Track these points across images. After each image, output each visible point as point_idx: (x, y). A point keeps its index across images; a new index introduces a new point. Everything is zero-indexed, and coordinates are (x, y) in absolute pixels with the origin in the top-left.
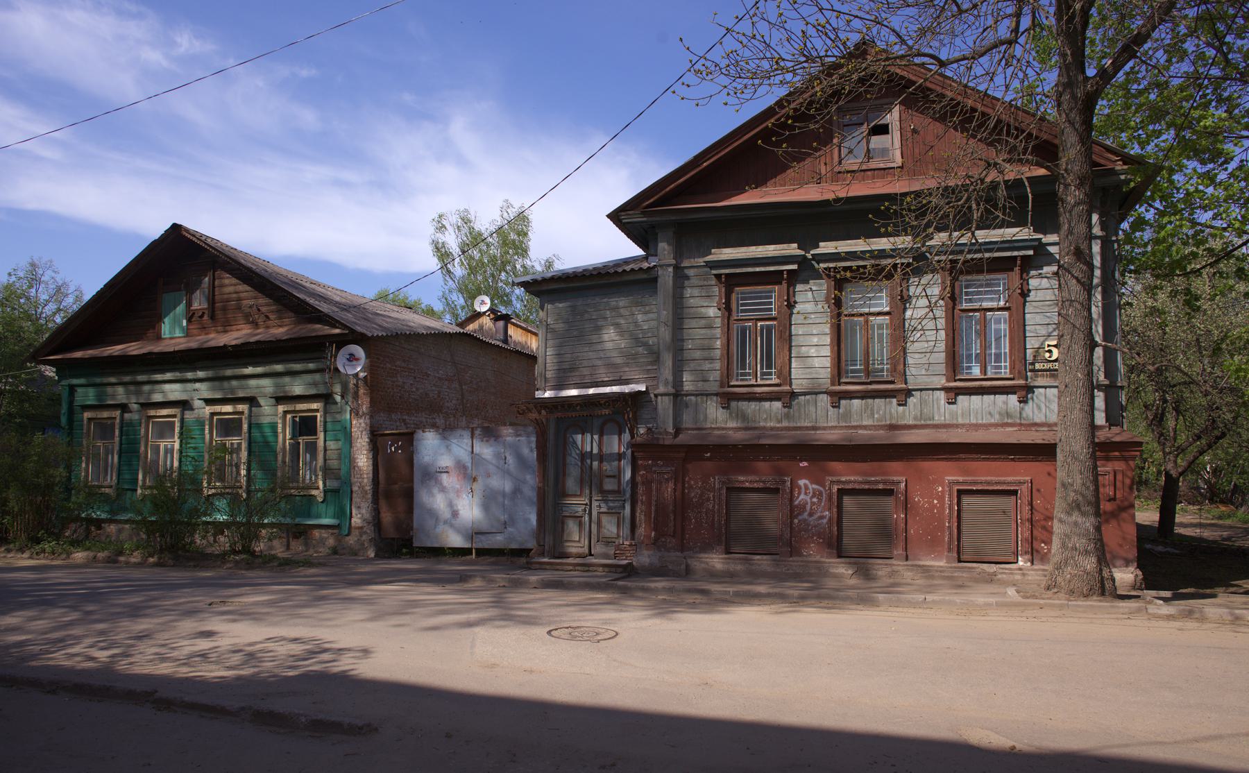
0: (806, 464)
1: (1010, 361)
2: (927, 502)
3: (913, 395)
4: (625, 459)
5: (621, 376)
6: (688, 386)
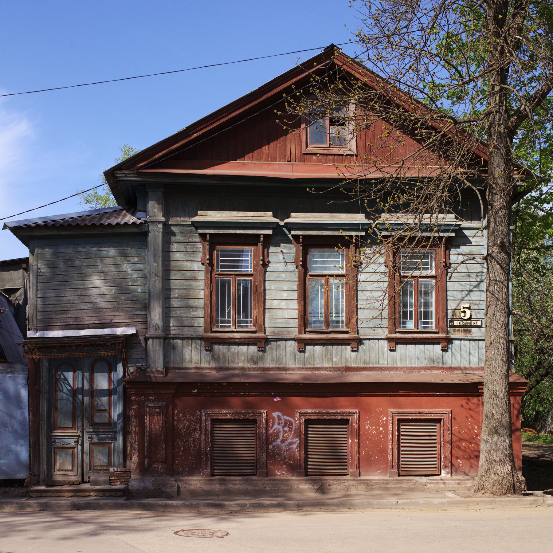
0: (278, 399)
1: (436, 319)
2: (375, 429)
3: (363, 344)
4: (115, 394)
5: (112, 320)
6: (173, 331)
